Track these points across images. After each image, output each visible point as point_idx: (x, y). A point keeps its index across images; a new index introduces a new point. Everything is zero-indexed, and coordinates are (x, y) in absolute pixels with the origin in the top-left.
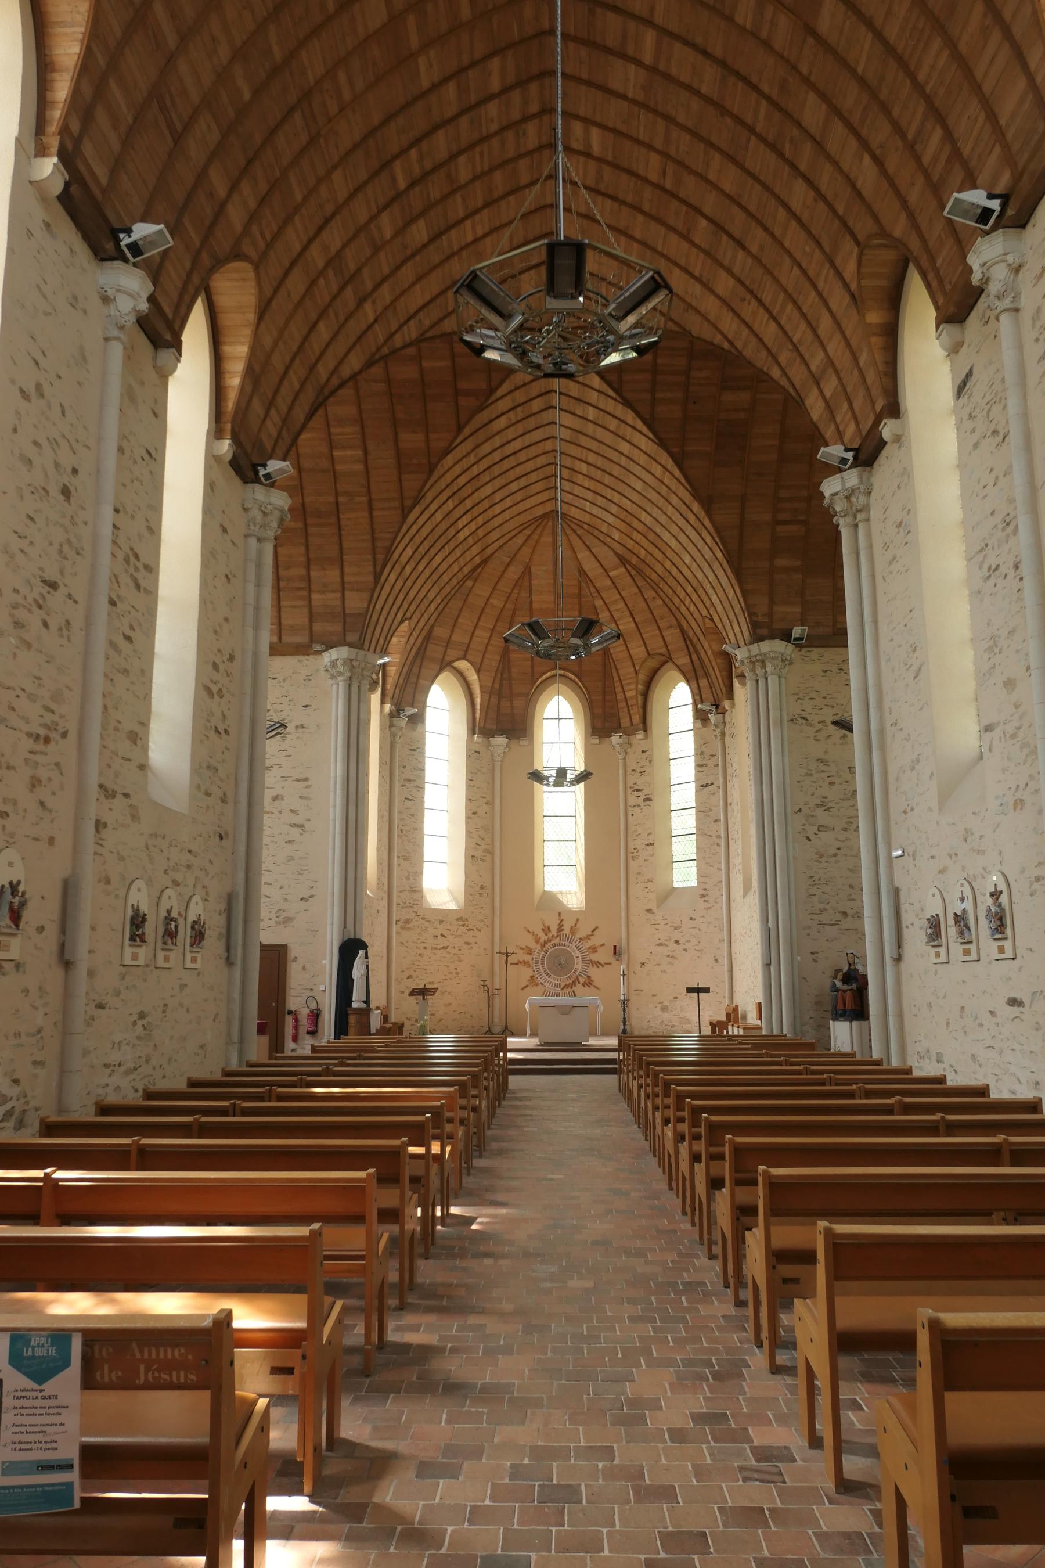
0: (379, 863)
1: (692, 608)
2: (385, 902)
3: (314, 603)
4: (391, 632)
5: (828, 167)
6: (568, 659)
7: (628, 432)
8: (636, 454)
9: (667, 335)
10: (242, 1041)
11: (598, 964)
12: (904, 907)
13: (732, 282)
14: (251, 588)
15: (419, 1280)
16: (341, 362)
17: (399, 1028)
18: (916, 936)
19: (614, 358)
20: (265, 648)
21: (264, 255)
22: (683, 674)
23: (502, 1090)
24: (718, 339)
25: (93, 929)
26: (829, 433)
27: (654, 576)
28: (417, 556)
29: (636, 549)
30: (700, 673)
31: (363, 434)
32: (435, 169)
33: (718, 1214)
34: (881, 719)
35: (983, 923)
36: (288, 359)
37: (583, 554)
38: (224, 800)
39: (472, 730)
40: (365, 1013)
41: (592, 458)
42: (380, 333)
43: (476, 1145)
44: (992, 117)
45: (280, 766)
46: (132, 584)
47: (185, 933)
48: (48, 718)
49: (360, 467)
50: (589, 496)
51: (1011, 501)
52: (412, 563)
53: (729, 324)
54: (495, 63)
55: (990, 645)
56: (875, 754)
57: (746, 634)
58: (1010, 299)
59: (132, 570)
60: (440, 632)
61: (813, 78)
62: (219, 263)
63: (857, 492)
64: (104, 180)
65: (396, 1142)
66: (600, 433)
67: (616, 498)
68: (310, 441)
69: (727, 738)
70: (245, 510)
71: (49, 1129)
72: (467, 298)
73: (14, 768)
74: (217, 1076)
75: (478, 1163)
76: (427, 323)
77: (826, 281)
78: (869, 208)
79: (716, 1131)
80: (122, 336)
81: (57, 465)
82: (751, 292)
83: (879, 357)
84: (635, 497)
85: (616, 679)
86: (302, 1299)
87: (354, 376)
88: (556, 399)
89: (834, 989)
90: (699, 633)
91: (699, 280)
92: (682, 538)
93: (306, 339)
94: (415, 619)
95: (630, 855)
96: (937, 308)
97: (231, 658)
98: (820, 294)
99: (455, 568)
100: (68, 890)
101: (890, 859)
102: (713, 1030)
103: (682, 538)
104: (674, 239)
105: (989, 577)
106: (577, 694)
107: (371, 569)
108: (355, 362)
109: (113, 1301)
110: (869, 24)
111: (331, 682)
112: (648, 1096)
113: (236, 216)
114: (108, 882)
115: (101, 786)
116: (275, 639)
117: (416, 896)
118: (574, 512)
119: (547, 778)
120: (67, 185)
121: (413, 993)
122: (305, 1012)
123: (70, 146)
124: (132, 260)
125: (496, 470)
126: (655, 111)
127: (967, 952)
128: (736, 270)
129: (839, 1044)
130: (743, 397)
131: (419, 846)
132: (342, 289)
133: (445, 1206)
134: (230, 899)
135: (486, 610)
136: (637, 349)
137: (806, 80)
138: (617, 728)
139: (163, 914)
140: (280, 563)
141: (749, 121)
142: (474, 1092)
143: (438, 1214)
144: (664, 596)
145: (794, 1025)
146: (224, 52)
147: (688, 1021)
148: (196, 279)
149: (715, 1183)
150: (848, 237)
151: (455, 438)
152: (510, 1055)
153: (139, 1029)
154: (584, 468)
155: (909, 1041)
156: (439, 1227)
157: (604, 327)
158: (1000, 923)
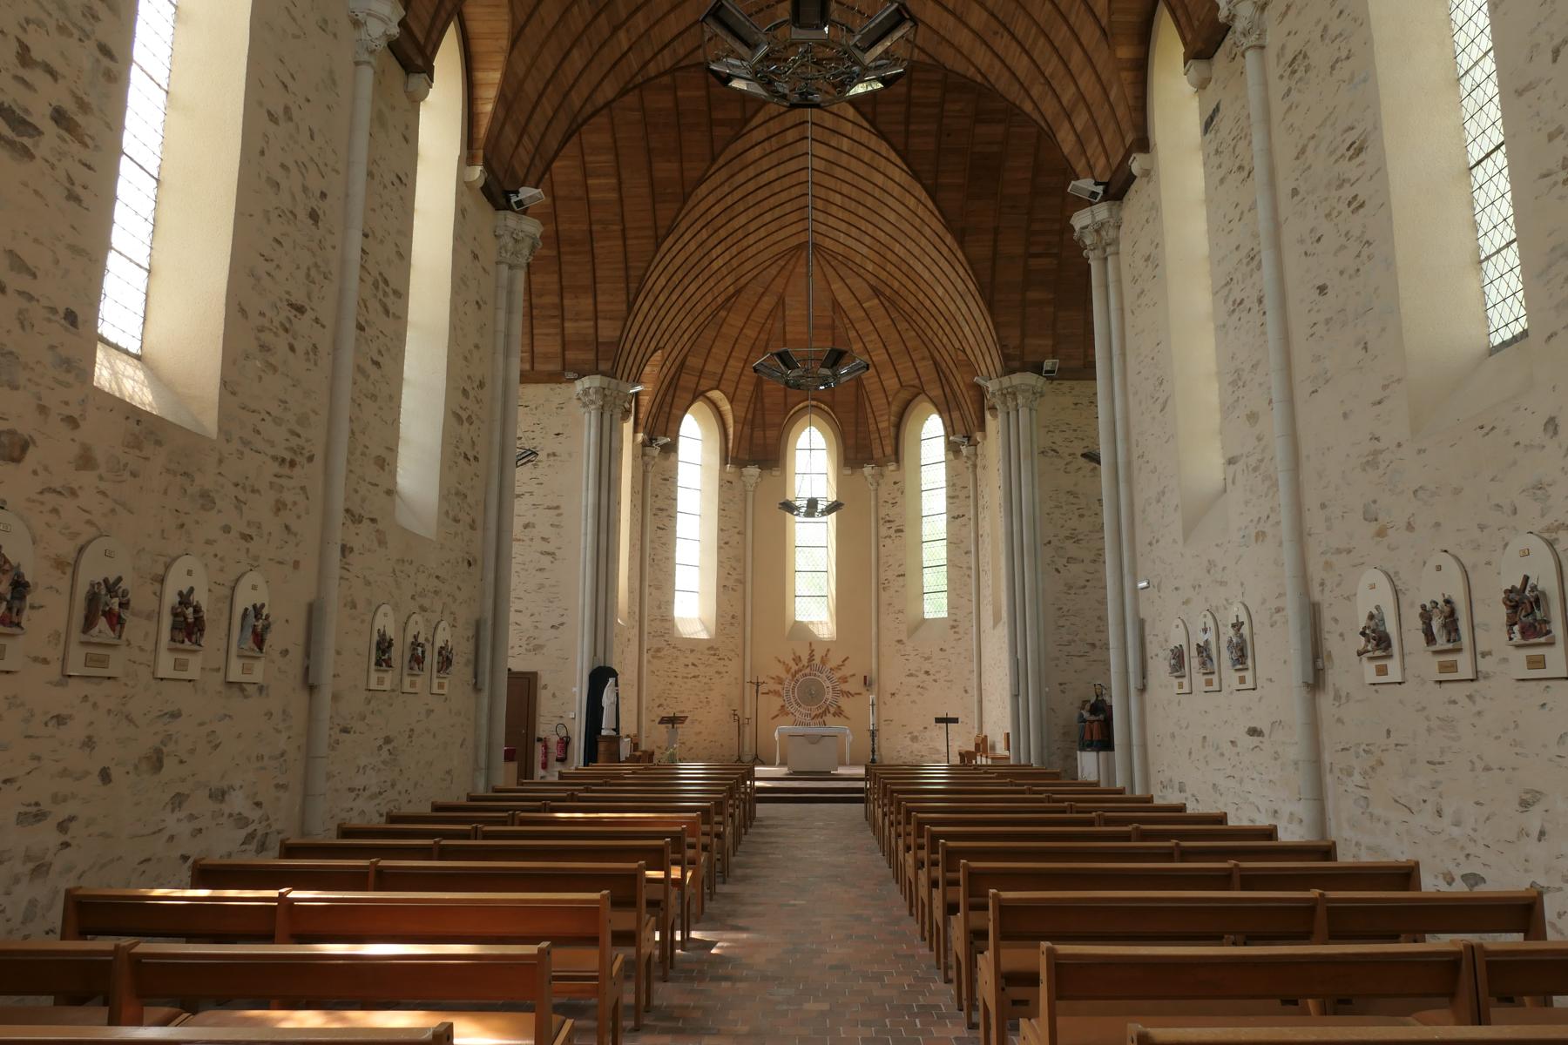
0: (631, 591)
1: (945, 340)
2: (636, 631)
8: (890, 185)
9: (913, 67)
10: (488, 768)
11: (848, 694)
12: (1149, 638)
13: (985, 15)
14: (502, 315)
15: (656, 1002)
16: (594, 91)
17: (650, 756)
18: (1160, 667)
19: (860, 89)
23: (749, 818)
24: (971, 72)
25: (338, 653)
26: (1080, 166)
27: (907, 307)
28: (671, 285)
33: (953, 938)
34: (1128, 450)
35: (1225, 654)
36: (541, 86)
37: (836, 286)
38: (472, 527)
39: (725, 458)
40: (615, 740)
41: (846, 189)
42: (634, 61)
43: (719, 872)
45: (531, 494)
46: (380, 309)
47: (432, 659)
48: (294, 442)
49: (614, 196)
50: (843, 226)
51: (1255, 236)
52: (666, 292)
53: (982, 57)
55: (1235, 381)
56: (1122, 486)
58: (1255, 36)
59: (380, 294)
60: (694, 362)
65: (634, 865)
66: (854, 165)
68: (563, 168)
69: (979, 470)
71: (289, 851)
72: (713, 28)
73: (258, 491)
74: (463, 801)
75: (722, 889)
76: (682, 52)
79: (952, 856)
80: (372, 60)
81: (305, 189)
82: (1004, 26)
84: (888, 228)
86: (530, 1018)
87: (608, 104)
88: (809, 131)
89: (1082, 720)
90: (951, 365)
91: (952, 13)
92: (935, 269)
93: (559, 66)
94: (668, 348)
95: (881, 586)
96: (1185, 44)
97: (481, 385)
99: (709, 298)
100: (313, 614)
101: (1135, 590)
102: (962, 759)
103: (935, 269)
108: (608, 91)
109: (343, 1019)
112: (891, 824)
114: (354, 606)
115: (347, 511)
116: (527, 367)
117: (667, 625)
118: (828, 243)
119: (798, 508)
121: (663, 721)
122: (555, 739)
125: (751, 200)
127: (1209, 683)
129: (1086, 774)
131: (671, 575)
133: (686, 930)
134: (478, 625)
138: (870, 460)
139: (410, 639)
142: (717, 819)
143: (678, 937)
145: (1041, 755)
147: (938, 752)
149: (951, 909)
152: (758, 784)
153: (385, 754)
154: (838, 199)
155: (1153, 770)
156: (678, 951)
157: (849, 58)
158: (1241, 654)
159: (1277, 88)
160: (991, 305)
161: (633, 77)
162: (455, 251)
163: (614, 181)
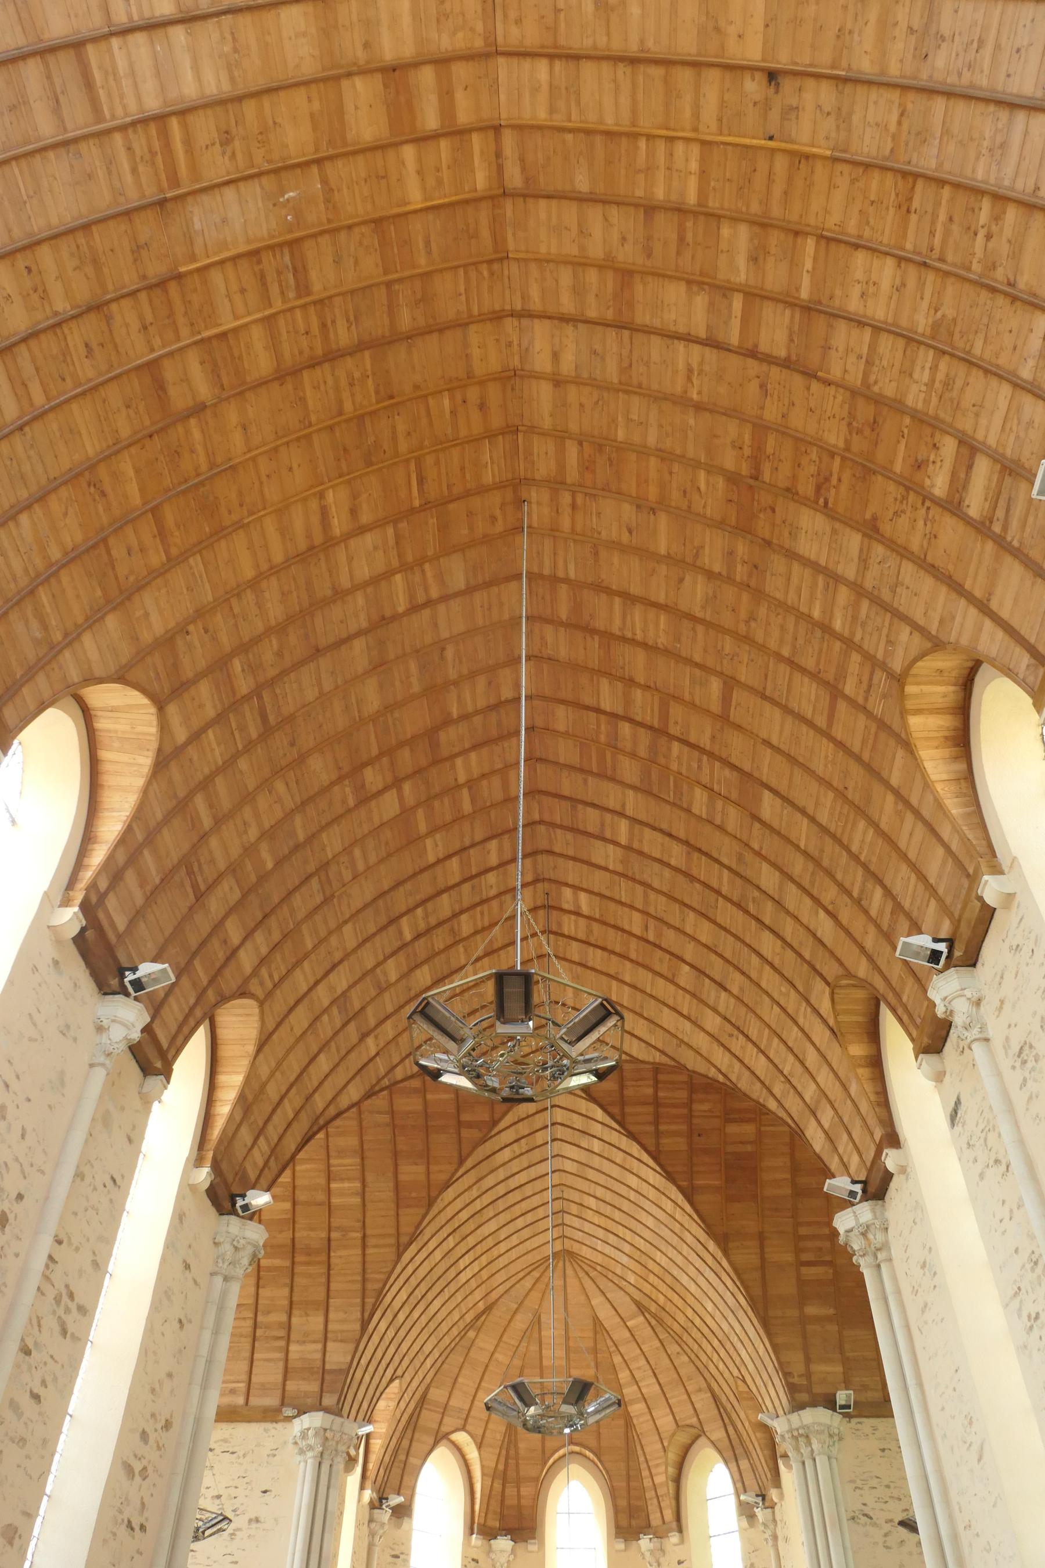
1: (721, 1366)
3: (291, 1356)
4: (378, 1394)
5: (789, 920)
6: (561, 1433)
7: (635, 1165)
8: (645, 1188)
13: (718, 1019)
14: (207, 1335)
20: (211, 1412)
21: (269, 994)
22: (720, 1452)
24: (712, 1073)
26: (834, 1164)
28: (413, 1300)
29: (654, 1295)
30: (739, 1451)
31: (363, 1165)
32: (439, 924)
36: (284, 1089)
37: (597, 1301)
41: (600, 1192)
42: (381, 1066)
44: (922, 877)
46: (57, 1329)
49: (358, 1200)
50: (600, 1233)
52: (407, 1309)
53: (721, 1058)
54: (493, 844)
57: (784, 1401)
59: (61, 1311)
60: (437, 1395)
61: (763, 852)
62: (224, 999)
63: (872, 1228)
64: (121, 927)
66: (607, 1166)
67: (628, 1235)
68: (307, 1169)
69: (781, 1543)
70: (216, 1244)
77: (805, 1017)
78: (832, 953)
80: (107, 1062)
82: (738, 1029)
83: (869, 1087)
84: (647, 1234)
85: (642, 1459)
87: (357, 1104)
91: (688, 1018)
94: (407, 1377)
96: (912, 1040)
97: (167, 1425)
98: (802, 1030)
104: (661, 982)
105: (1031, 1327)
106: (595, 1478)
107: (359, 1315)
108: (354, 1093)
110: (803, 812)
111: (299, 1458)
113: (247, 959)
118: (585, 1252)
120: (83, 930)
123: (94, 899)
124: (133, 994)
125: (501, 1205)
126: (633, 880)
128: (721, 1009)
130: (748, 1130)
132: (345, 1025)
135: (490, 1368)
136: (596, 1073)
137: (758, 854)
138: (646, 1528)
140: (260, 1307)
141: (715, 885)
144: (689, 1351)
146: (253, 833)
148: (198, 1013)
150: (818, 979)
151: (457, 1170)
154: (592, 1203)
159: (1013, 1079)
160: (766, 1323)
161: (379, 1081)
162: (164, 1260)
163: (358, 1185)
